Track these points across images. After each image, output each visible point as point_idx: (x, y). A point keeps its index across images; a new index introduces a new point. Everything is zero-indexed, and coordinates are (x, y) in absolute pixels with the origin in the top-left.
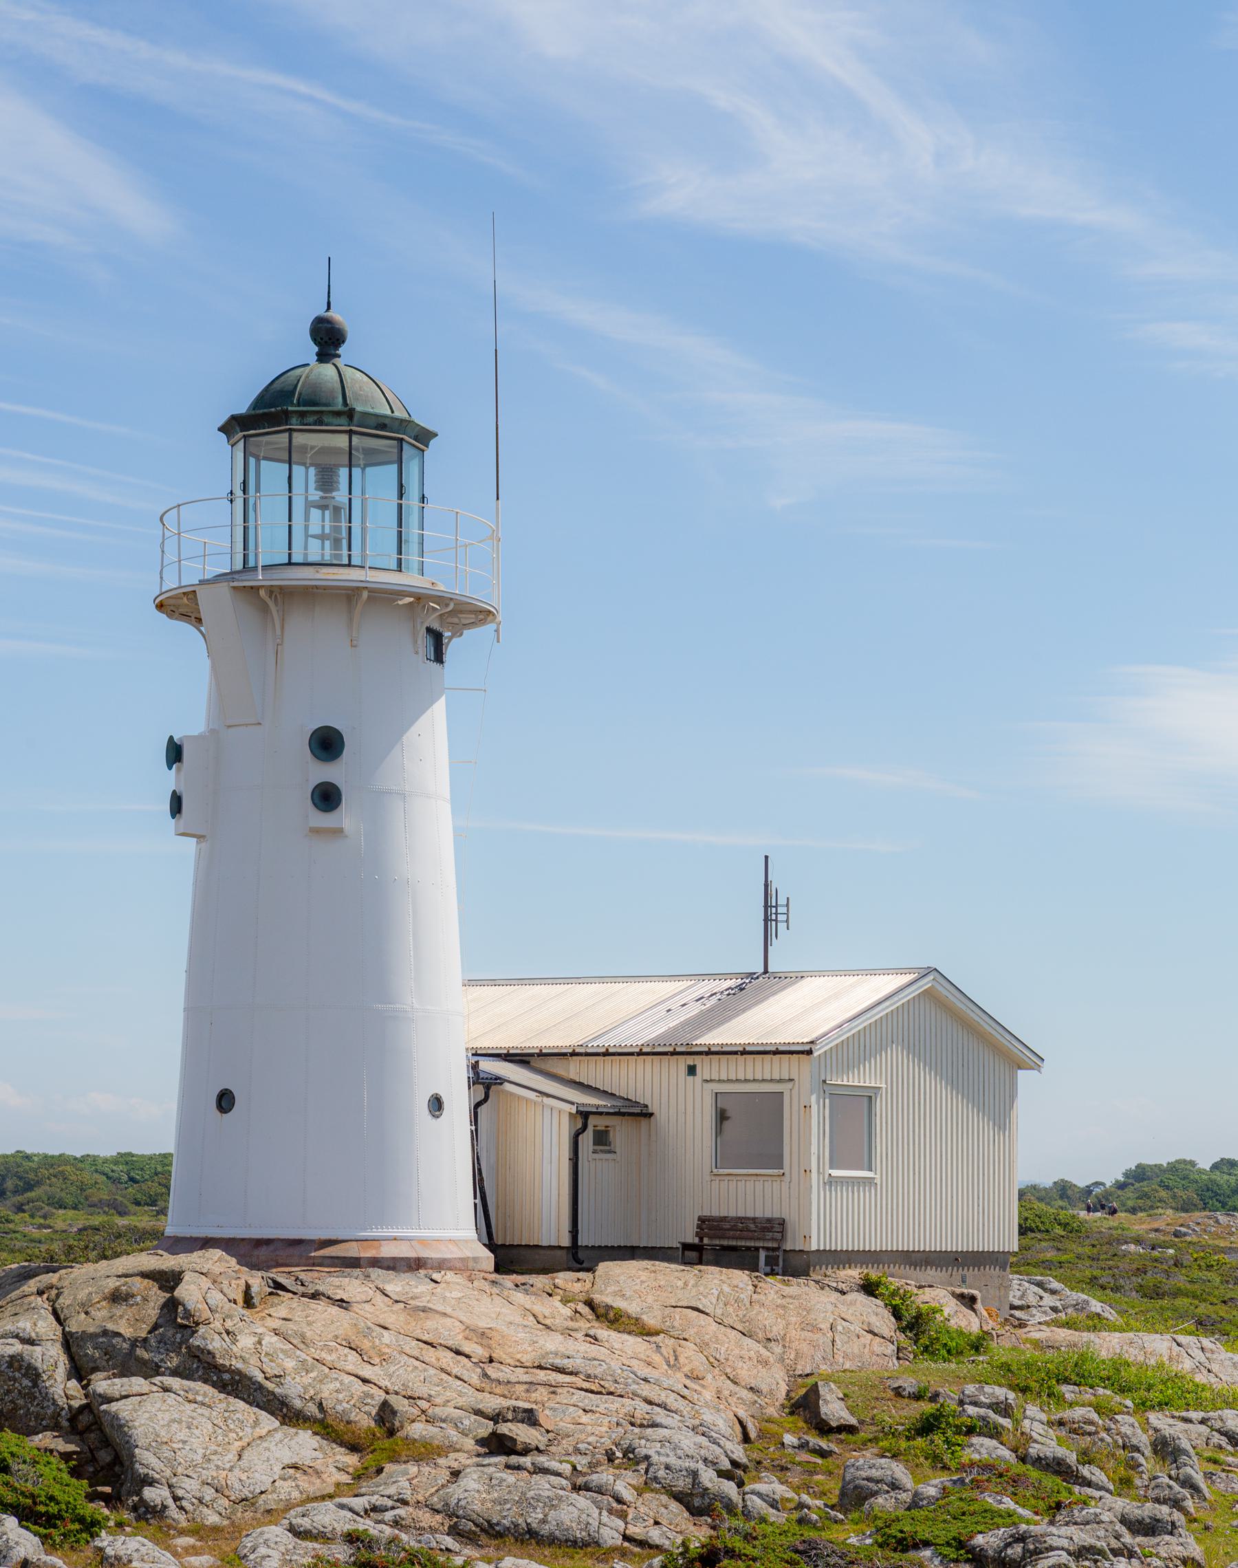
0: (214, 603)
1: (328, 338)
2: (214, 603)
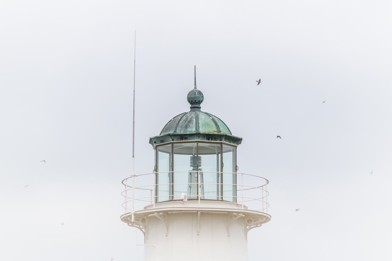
0: (259, 82)
1: (195, 101)
2: (259, 82)
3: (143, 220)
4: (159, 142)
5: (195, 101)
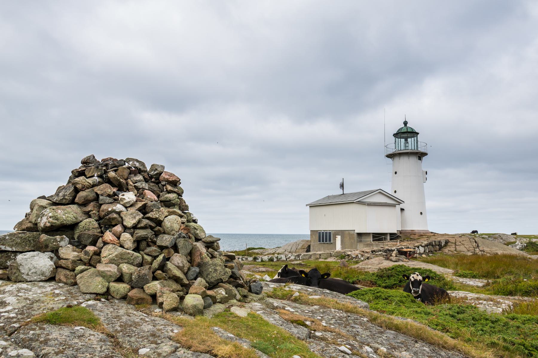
1: (405, 123)
3: (391, 156)
4: (396, 135)
5: (405, 123)
